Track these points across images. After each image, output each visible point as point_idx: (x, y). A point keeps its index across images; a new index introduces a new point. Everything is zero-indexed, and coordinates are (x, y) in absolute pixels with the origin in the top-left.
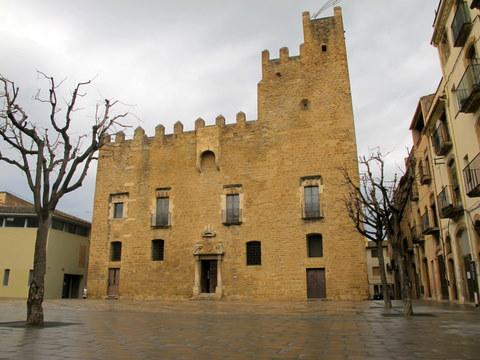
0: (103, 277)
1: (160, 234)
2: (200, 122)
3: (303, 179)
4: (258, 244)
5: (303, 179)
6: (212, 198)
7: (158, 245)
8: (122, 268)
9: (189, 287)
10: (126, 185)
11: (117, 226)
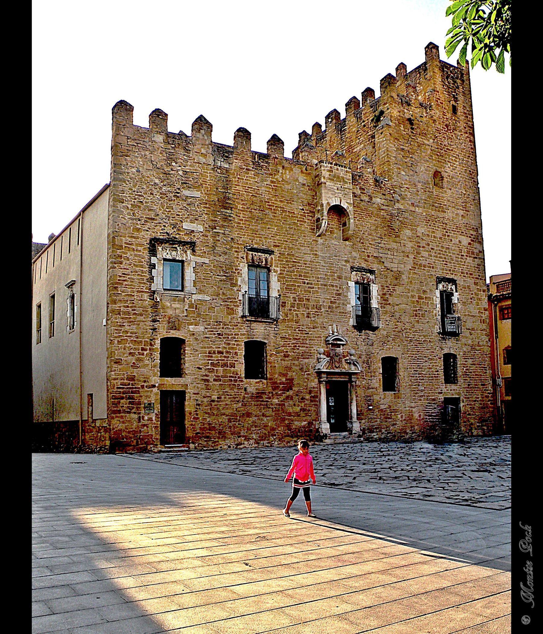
0: (149, 406)
1: (260, 331)
2: (202, 124)
3: (440, 280)
4: (454, 356)
5: (440, 280)
6: (335, 283)
7: (255, 352)
8: (190, 391)
9: (310, 424)
10: (186, 226)
11: (172, 308)
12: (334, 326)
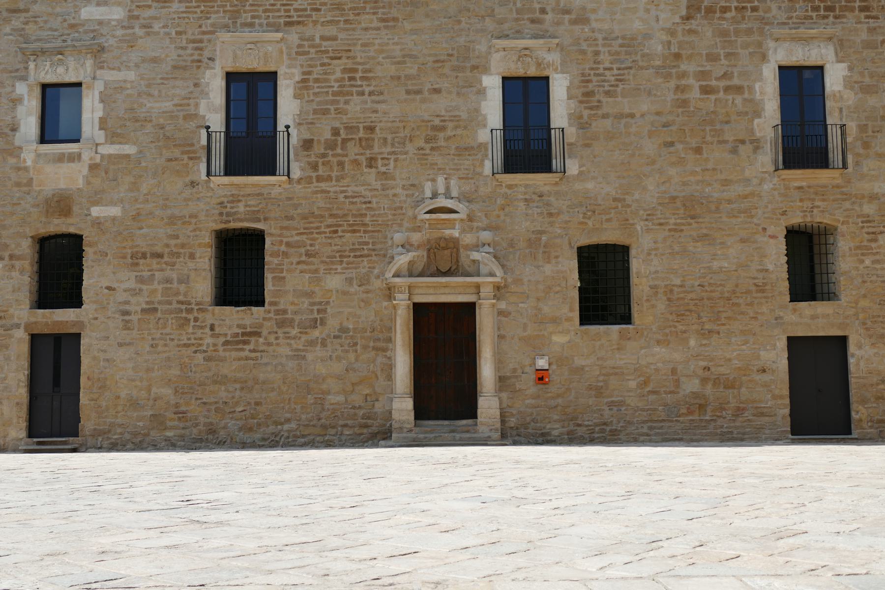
12: (441, 180)
